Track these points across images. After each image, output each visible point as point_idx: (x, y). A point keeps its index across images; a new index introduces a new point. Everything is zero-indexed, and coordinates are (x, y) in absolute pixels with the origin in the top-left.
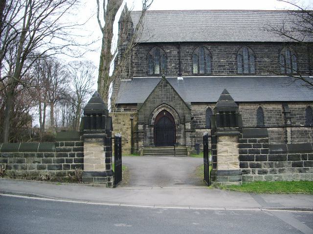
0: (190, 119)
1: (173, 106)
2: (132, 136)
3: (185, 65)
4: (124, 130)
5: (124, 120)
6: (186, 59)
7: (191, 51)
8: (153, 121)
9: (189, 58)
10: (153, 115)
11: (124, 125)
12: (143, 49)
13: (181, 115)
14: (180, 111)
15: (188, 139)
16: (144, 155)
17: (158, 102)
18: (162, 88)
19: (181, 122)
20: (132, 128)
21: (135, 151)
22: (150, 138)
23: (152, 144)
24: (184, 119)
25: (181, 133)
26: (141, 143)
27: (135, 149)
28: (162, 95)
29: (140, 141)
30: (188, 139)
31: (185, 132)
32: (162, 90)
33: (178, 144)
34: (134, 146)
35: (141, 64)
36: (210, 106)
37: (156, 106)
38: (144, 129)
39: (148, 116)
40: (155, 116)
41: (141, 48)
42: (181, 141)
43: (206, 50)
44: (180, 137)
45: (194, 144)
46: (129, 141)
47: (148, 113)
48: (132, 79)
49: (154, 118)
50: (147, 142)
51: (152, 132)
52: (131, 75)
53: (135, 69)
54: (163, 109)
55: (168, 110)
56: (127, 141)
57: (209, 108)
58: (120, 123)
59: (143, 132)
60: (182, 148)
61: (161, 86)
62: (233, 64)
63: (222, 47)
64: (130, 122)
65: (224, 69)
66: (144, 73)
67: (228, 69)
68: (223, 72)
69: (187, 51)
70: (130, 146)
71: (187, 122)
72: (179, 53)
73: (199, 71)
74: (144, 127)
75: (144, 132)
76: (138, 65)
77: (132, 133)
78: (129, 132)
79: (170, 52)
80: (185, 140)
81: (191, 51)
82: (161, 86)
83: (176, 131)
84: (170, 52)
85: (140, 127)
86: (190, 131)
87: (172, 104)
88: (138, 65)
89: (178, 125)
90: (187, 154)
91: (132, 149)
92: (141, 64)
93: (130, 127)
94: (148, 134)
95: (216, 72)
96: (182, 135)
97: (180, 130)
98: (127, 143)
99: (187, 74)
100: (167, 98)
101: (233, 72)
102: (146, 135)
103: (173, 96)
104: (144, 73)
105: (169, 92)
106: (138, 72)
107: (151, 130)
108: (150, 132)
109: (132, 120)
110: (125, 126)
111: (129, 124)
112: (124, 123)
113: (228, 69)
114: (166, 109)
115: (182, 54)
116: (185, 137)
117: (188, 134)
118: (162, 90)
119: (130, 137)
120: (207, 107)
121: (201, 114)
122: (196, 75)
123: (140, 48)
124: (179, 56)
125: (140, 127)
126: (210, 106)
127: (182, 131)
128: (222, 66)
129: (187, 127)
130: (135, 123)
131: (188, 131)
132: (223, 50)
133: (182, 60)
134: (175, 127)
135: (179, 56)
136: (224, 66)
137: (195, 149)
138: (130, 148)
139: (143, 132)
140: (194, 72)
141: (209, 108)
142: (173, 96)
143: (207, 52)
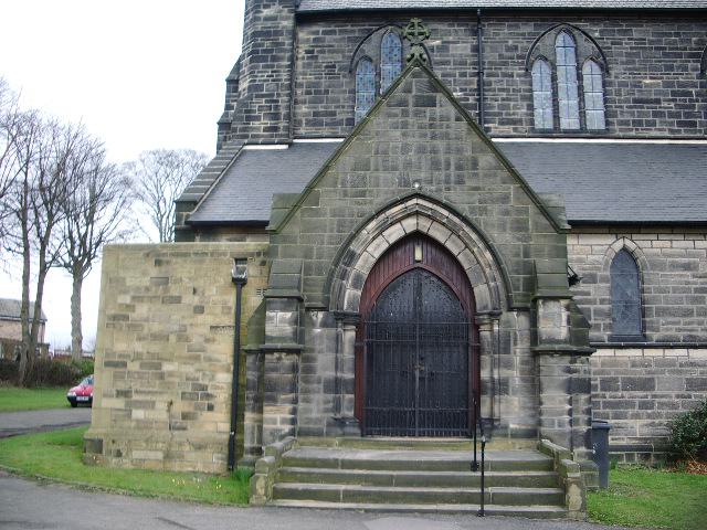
0: (562, 279)
1: (464, 209)
2: (237, 374)
3: (504, 95)
4: (196, 340)
5: (200, 283)
6: (505, 75)
7: (524, 44)
8: (351, 295)
9: (518, 71)
10: (352, 257)
11: (200, 310)
12: (338, 36)
13: (509, 261)
14: (504, 239)
15: (555, 400)
16: (279, 494)
17: (385, 186)
18: (405, 114)
19: (509, 299)
20: (237, 327)
21: (248, 457)
22: (335, 386)
23: (341, 422)
24: (532, 284)
25: (509, 365)
26: (277, 416)
27: (247, 445)
28: (405, 149)
29: (273, 400)
30: (555, 400)
31: (535, 355)
32: (405, 125)
33: (492, 426)
34: (242, 432)
35: (327, 92)
36: (628, 243)
37: (370, 209)
38: (299, 336)
39: (327, 261)
40: (363, 265)
41: (332, 32)
42: (511, 410)
43: (581, 39)
44: (501, 387)
45: (584, 428)
46: (223, 397)
47: (326, 248)
48: (291, 144)
49: (358, 278)
50: (316, 408)
51: (348, 354)
52: (287, 128)
53: (303, 109)
54: (410, 225)
55: (438, 234)
56: (209, 396)
57: (625, 249)
58: (178, 300)
59: (289, 351)
60: (522, 452)
61: (403, 103)
62: (690, 94)
63: (640, 32)
64: (231, 299)
65: (655, 114)
66: (340, 123)
67: (671, 115)
68: (654, 124)
69: (510, 42)
70: (225, 426)
71: (547, 299)
72: (476, 49)
73: (556, 117)
74: (301, 322)
75: (299, 348)
76: (316, 92)
77: (239, 355)
78: (223, 349)
79: (444, 48)
80: (536, 406)
81: (524, 44)
82: (403, 103)
83: (479, 351)
84: (444, 48)
85: (280, 322)
86: (564, 353)
87: (458, 197)
88: (316, 92)
89: (494, 315)
90: (560, 500)
91: (232, 439)
92: (327, 92)
93: (230, 320)
94: (324, 366)
95: (626, 123)
96: (515, 376)
97: (503, 344)
98: (211, 408)
99: (508, 129)
100: (435, 165)
101: (694, 124)
102: (309, 370)
103: (469, 154)
104: (340, 123)
105: (446, 136)
106: (315, 121)
107: (338, 348)
108: (334, 351)
109: (239, 283)
110: (200, 318)
111: (225, 309)
112: (196, 300)
113: (671, 115)
114: (424, 225)
115: (489, 56)
116: (534, 386)
117: (554, 368)
118: (405, 125)
119: (225, 378)
120: (619, 245)
121: (592, 279)
122: (545, 134)
123: (325, 33)
124: (479, 64)
125: (280, 322)
126: (628, 243)
127: (519, 351)
128: (647, 101)
129: (545, 328)
130: (253, 300)
131: (551, 353)
132: (651, 42)
133: (489, 75)
134: (477, 327)
135: (479, 64)
136: (658, 101)
137: (591, 456)
138: (226, 437)
139: (289, 351)
140: (539, 124)
141: (625, 249)
142: (469, 154)
143: (588, 47)
